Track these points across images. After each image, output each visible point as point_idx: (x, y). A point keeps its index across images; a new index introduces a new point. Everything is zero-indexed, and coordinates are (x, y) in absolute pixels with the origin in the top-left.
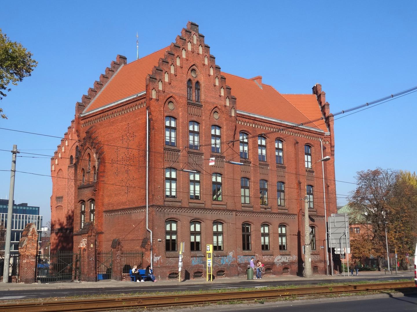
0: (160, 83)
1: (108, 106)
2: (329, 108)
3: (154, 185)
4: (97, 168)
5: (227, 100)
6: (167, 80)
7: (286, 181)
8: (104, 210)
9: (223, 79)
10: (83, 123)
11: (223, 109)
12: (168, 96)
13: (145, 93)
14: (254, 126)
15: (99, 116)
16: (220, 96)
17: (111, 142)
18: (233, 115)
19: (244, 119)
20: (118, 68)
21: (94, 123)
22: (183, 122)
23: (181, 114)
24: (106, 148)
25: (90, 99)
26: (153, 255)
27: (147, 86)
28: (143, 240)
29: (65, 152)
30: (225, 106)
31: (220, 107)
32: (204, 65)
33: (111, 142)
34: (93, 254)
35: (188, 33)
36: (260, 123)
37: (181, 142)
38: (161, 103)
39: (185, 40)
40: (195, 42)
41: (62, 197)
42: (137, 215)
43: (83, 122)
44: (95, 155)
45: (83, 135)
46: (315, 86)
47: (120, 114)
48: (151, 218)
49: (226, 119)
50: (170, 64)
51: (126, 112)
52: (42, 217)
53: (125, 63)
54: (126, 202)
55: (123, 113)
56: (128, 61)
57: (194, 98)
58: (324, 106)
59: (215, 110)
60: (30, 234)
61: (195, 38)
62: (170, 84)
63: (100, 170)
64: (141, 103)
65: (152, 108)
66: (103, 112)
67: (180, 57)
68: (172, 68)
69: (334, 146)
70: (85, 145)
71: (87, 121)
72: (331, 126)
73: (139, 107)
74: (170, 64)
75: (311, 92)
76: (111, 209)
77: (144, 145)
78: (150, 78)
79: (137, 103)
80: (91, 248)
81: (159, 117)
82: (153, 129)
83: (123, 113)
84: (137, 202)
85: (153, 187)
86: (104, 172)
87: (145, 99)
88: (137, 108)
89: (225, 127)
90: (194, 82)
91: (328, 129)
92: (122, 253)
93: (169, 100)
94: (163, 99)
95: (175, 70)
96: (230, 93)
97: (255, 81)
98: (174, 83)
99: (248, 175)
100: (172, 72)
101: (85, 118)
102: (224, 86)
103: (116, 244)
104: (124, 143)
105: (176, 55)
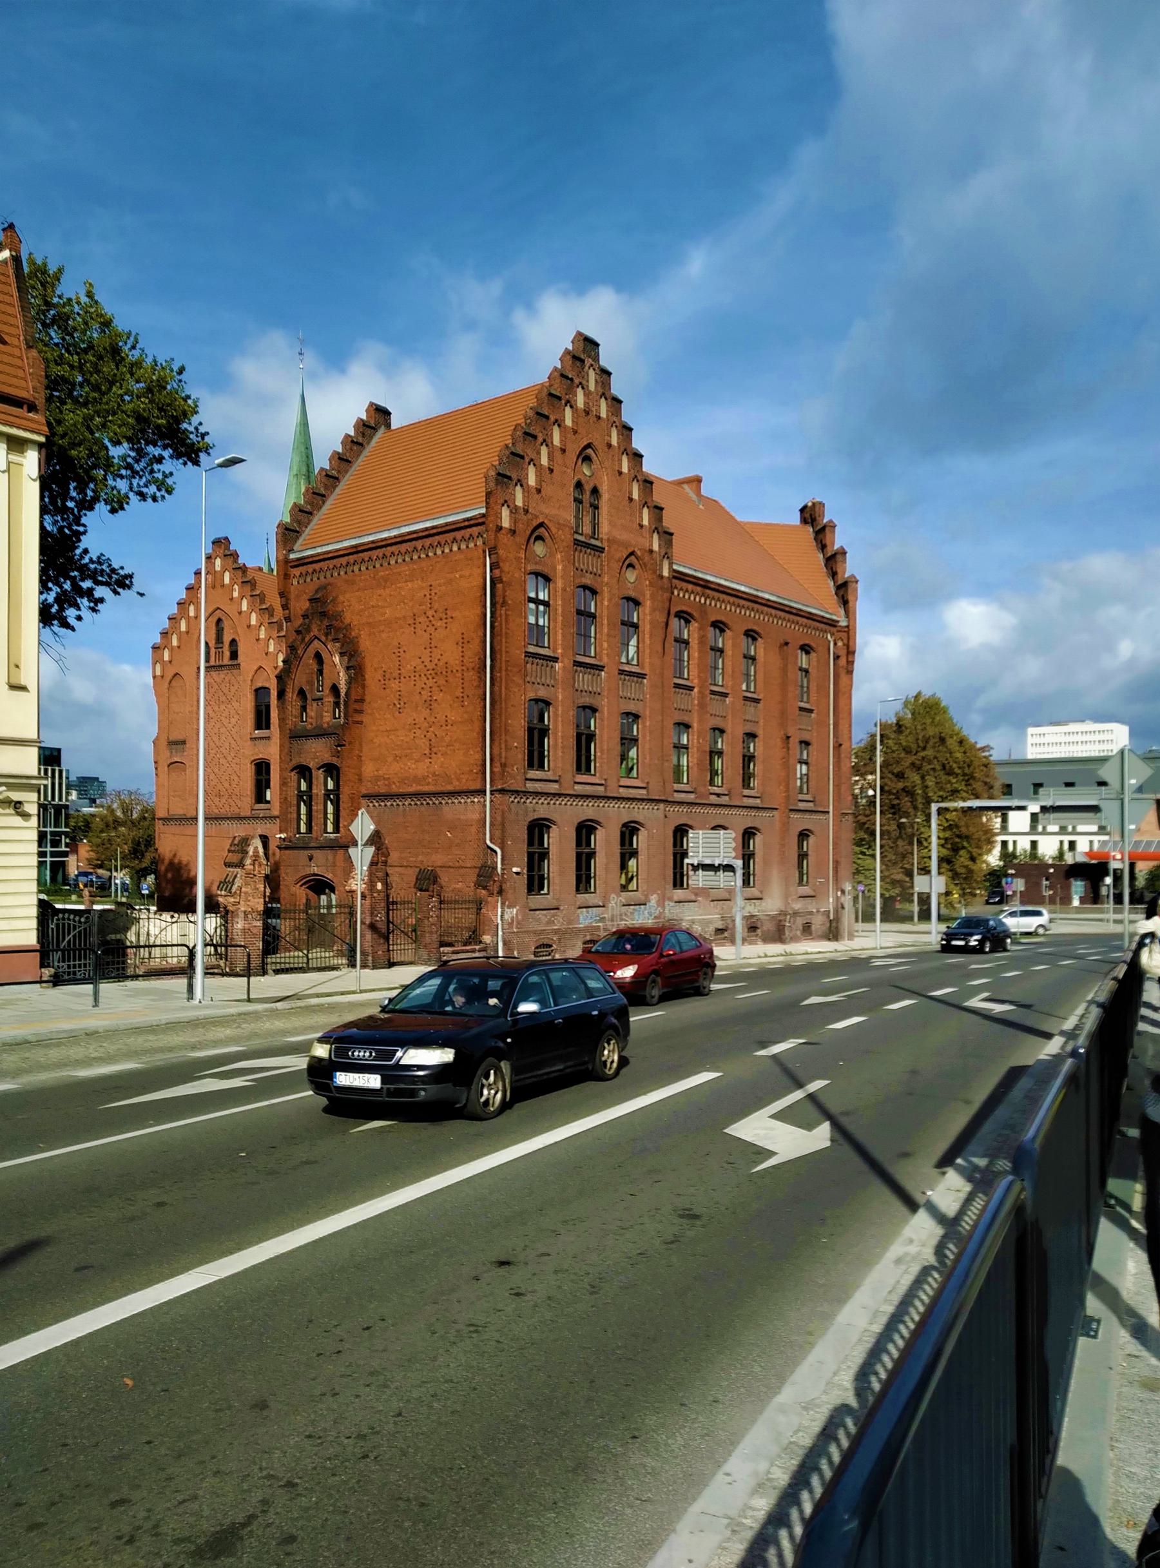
0: (518, 488)
1: (371, 538)
2: (844, 561)
3: (506, 741)
4: (343, 692)
5: (655, 536)
6: (532, 481)
7: (760, 732)
8: (364, 791)
9: (648, 483)
10: (298, 574)
11: (647, 558)
12: (535, 523)
13: (483, 511)
14: (703, 601)
15: (344, 560)
16: (641, 526)
17: (382, 628)
18: (666, 573)
19: (684, 585)
20: (371, 438)
21: (328, 575)
22: (564, 590)
23: (560, 567)
24: (365, 643)
25: (311, 513)
26: (503, 904)
27: (489, 494)
28: (481, 868)
29: (187, 632)
30: (651, 551)
31: (639, 553)
32: (610, 446)
33: (382, 628)
34: (383, 905)
35: (578, 364)
36: (716, 595)
37: (560, 637)
38: (521, 539)
39: (572, 380)
40: (592, 386)
41: (184, 742)
42: (456, 809)
43: (296, 572)
44: (337, 659)
45: (301, 605)
46: (810, 504)
47: (407, 559)
48: (499, 819)
49: (651, 585)
50: (540, 439)
51: (423, 556)
52: (68, 771)
53: (388, 426)
54: (425, 778)
55: (415, 557)
56: (396, 422)
57: (587, 529)
58: (834, 556)
59: (630, 561)
60: (248, 861)
61: (592, 375)
62: (539, 491)
63: (353, 696)
64: (467, 536)
65: (501, 552)
66: (356, 550)
67: (559, 423)
68: (544, 451)
69: (854, 653)
70: (308, 630)
71: (310, 571)
72: (851, 604)
73: (463, 546)
74: (540, 439)
75: (795, 519)
76: (383, 791)
77: (477, 641)
78: (499, 474)
79: (458, 535)
80: (379, 892)
81: (516, 575)
82: (504, 603)
83: (415, 557)
84: (458, 780)
85: (503, 746)
86: (362, 701)
87: (482, 528)
88: (455, 548)
89: (648, 603)
90: (588, 488)
91: (842, 612)
92: (441, 902)
93: (538, 532)
94: (524, 530)
95: (551, 457)
96: (660, 519)
97: (686, 486)
98: (547, 490)
99: (686, 719)
100: (544, 461)
101: (301, 562)
102: (649, 501)
103: (427, 880)
104: (420, 632)
105: (552, 419)
